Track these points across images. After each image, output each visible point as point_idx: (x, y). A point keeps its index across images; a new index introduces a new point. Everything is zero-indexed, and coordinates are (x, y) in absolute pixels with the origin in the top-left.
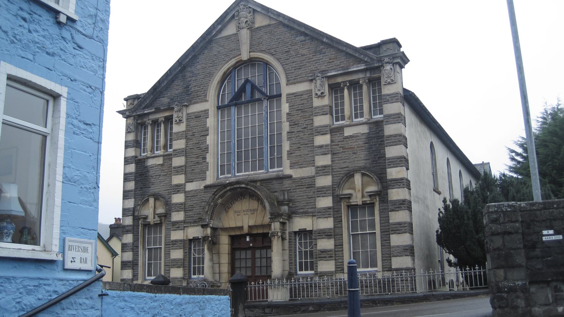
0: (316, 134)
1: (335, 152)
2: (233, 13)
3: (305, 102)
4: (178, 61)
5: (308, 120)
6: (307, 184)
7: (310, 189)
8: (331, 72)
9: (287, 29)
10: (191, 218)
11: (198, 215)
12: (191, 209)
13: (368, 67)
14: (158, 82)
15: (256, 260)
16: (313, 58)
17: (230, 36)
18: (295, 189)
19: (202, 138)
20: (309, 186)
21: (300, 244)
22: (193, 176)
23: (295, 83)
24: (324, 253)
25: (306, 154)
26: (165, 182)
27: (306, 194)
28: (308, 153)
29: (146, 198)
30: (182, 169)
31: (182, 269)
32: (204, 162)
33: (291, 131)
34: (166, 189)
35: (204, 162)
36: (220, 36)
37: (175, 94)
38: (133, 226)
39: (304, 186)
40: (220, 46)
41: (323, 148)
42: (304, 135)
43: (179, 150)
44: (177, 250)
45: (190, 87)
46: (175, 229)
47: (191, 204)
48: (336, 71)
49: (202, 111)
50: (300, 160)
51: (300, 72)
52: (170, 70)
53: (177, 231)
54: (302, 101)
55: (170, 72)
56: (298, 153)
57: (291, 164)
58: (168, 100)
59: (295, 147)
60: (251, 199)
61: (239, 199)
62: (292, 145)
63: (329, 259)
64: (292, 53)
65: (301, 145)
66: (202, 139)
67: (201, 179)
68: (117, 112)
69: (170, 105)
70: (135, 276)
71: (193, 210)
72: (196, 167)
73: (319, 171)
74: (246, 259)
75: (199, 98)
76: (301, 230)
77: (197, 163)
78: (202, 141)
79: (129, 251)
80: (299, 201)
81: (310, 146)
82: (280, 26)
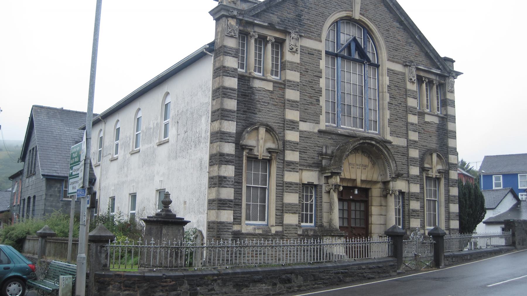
5: (402, 98)
6: (402, 152)
7: (404, 157)
10: (305, 161)
11: (312, 159)
12: (305, 151)
13: (442, 73)
15: (352, 211)
16: (405, 47)
23: (393, 62)
24: (414, 212)
26: (275, 113)
27: (401, 160)
29: (257, 126)
30: (297, 105)
34: (277, 122)
38: (236, 156)
39: (399, 153)
42: (399, 110)
43: (294, 82)
46: (290, 169)
47: (305, 146)
48: (423, 67)
49: (315, 50)
53: (292, 173)
54: (398, 80)
56: (395, 123)
58: (278, 20)
59: (394, 117)
62: (392, 115)
63: (418, 217)
64: (390, 33)
65: (398, 117)
66: (316, 80)
67: (316, 122)
68: (463, 73)
69: (286, 28)
70: (237, 220)
71: (306, 152)
78: (316, 82)
79: (230, 187)
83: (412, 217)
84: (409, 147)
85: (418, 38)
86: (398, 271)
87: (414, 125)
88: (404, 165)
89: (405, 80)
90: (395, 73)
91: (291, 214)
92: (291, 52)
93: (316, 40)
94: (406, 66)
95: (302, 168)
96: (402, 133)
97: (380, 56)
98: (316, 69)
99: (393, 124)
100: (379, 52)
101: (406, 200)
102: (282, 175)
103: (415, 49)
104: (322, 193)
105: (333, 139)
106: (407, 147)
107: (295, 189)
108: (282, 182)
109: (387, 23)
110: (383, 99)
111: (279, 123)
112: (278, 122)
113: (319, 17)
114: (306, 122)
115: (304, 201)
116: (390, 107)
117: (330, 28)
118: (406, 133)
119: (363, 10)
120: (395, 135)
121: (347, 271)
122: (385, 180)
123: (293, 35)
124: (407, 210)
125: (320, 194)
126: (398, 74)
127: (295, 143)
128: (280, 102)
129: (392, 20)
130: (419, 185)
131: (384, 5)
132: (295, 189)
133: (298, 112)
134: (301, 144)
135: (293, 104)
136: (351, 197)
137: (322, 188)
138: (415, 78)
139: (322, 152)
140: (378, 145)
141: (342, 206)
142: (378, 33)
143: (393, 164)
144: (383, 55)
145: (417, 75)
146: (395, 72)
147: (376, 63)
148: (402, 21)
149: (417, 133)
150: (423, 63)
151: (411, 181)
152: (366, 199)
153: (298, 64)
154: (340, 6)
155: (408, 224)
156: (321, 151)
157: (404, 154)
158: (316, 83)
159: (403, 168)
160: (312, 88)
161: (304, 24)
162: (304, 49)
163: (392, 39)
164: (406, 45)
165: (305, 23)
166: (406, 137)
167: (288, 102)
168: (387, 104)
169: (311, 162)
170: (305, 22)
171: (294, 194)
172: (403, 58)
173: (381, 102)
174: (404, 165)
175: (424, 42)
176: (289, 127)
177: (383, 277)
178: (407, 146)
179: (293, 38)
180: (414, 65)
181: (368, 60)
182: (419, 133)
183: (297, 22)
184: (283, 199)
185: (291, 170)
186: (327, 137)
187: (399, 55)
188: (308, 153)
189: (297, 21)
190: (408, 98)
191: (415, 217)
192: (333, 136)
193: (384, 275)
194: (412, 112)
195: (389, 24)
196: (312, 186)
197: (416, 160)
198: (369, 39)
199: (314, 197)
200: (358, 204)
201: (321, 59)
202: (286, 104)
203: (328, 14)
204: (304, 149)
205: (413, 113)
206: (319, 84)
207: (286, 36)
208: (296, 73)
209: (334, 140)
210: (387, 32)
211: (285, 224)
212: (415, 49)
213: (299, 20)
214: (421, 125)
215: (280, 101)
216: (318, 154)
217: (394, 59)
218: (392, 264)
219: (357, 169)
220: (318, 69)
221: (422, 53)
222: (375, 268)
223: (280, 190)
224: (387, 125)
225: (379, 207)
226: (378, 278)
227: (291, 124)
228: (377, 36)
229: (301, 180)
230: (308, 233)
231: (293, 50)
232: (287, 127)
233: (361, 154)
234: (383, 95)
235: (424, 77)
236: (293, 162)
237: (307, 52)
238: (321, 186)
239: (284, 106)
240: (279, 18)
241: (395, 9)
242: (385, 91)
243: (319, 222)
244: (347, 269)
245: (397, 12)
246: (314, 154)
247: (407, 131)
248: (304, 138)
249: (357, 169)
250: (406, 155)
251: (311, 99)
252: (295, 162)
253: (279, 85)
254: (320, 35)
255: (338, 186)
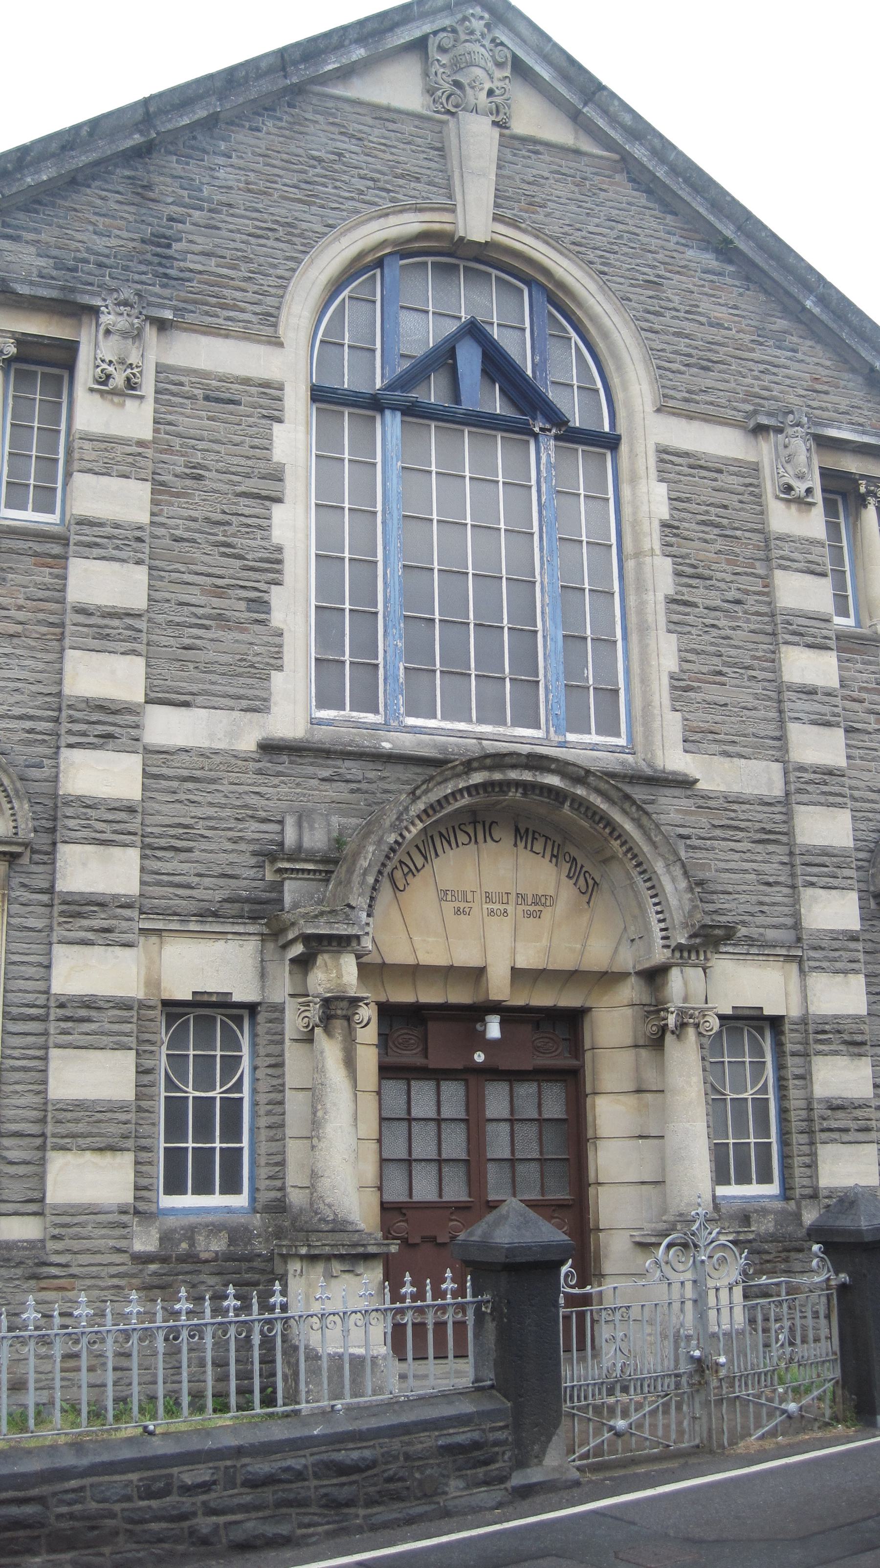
0: (789, 637)
1: (855, 725)
2: (427, 28)
3: (733, 500)
4: (146, 102)
5: (746, 574)
6: (758, 826)
7: (771, 848)
8: (839, 428)
9: (648, 200)
10: (180, 892)
11: (222, 882)
12: (179, 844)
14: (649, 125)
15: (490, 1128)
16: (753, 350)
17: (395, 116)
18: (709, 839)
19: (245, 506)
20: (767, 837)
21: (177, 1062)
22: (192, 680)
23: (690, 416)
24: (840, 1114)
25: (749, 705)
27: (754, 866)
28: (751, 702)
30: (130, 628)
31: (127, 1159)
32: (258, 621)
33: (679, 597)
34: (17, 711)
35: (258, 621)
36: (339, 91)
37: (88, 250)
40: (341, 133)
41: (815, 697)
43: (117, 526)
44: (98, 1053)
45: (176, 246)
49: (246, 381)
50: (723, 723)
51: (707, 380)
52: (95, 124)
55: (91, 134)
56: (713, 693)
57: (687, 729)
58: (42, 262)
60: (521, 845)
61: (462, 838)
63: (861, 1136)
64: (669, 294)
65: (725, 664)
66: (247, 511)
67: (244, 703)
69: (73, 290)
71: (190, 850)
72: (210, 634)
73: (806, 783)
74: (439, 1121)
75: (227, 313)
76: (740, 1012)
77: (220, 617)
80: (730, 888)
81: (764, 680)
82: (618, 177)
83: (825, 1136)
84: (794, 798)
85: (817, 310)
86: (517, 1479)
87: (818, 697)
88: (768, 884)
89: (759, 496)
90: (701, 467)
91: (88, 1155)
92: (101, 393)
93: (247, 337)
94: (759, 430)
95: (160, 925)
96: (755, 735)
97: (619, 396)
98: (250, 463)
99: (699, 696)
100: (615, 381)
101: (793, 1054)
102: (40, 965)
103: (808, 359)
104: (282, 1042)
105: (347, 781)
106: (786, 801)
107: (116, 1027)
108: (41, 1000)
109: (650, 255)
110: (641, 588)
111: (31, 718)
112: (24, 711)
113: (270, 243)
114: (186, 704)
115: (190, 1089)
116: (676, 618)
117: (345, 293)
118: (777, 734)
119: (516, 205)
120: (716, 748)
121: (29, 1510)
122: (647, 965)
123: (106, 319)
124: (802, 1104)
125: (272, 1049)
126: (720, 471)
127: (115, 809)
128: (39, 622)
129: (674, 239)
130: (861, 979)
131: (632, 180)
132: (116, 1027)
133: (139, 663)
134: (158, 813)
135: (106, 626)
136: (479, 1057)
137: (281, 1021)
138: (816, 482)
139: (281, 844)
140: (580, 791)
141: (433, 1103)
142: (600, 297)
143: (674, 880)
144: (635, 389)
145: (826, 473)
146: (702, 463)
147: (607, 428)
148: (727, 241)
149: (840, 732)
150: (855, 419)
151: (813, 964)
152: (570, 1062)
153: (141, 443)
154: (388, 191)
155: (808, 1171)
156: (272, 842)
157: (770, 832)
158: (249, 526)
159: (766, 899)
160: (223, 549)
161: (187, 275)
162: (183, 379)
163: (678, 318)
164: (761, 344)
165: (191, 271)
166: (778, 754)
167: (81, 619)
168: (661, 607)
169: (218, 896)
170: (192, 266)
171: (108, 1054)
172: (744, 401)
173: (632, 600)
174: (768, 884)
175: (848, 323)
176: (84, 734)
177: (374, 1528)
178: (787, 794)
179: (108, 332)
180: (798, 424)
181: (556, 418)
182: (849, 730)
183: (143, 268)
184: (45, 1082)
185: (90, 936)
186: (311, 770)
187: (720, 385)
188: (197, 853)
189: (150, 263)
190: (778, 574)
191: (846, 1137)
192: (348, 763)
193: (384, 1513)
194: (801, 635)
195: (659, 257)
196: (760, 1023)
197: (834, 859)
198: (565, 330)
199: (246, 1064)
200: (526, 1090)
201: (280, 421)
202: (70, 629)
203: (319, 228)
204: (172, 837)
205: (810, 640)
206: (267, 528)
207: (79, 325)
208: (132, 484)
209: (354, 786)
210: (651, 293)
211: (55, 1206)
212: (808, 359)
213: (156, 260)
214: (864, 695)
215: (41, 616)
216: (255, 854)
217: (692, 407)
218: (462, 1436)
219: (486, 919)
220: (262, 464)
221: (846, 376)
222: (300, 1476)
223: (31, 1039)
224: (666, 701)
225: (632, 1100)
226: (330, 1535)
227: (94, 719)
228: (598, 309)
229: (153, 982)
230: (192, 1245)
231: (112, 384)
232: (70, 732)
233: (507, 840)
234: (639, 566)
235: (863, 477)
236: (100, 899)
237: (198, 392)
238: (279, 1009)
239: (61, 638)
240: (48, 257)
241: (684, 193)
242: (647, 547)
243: (268, 1189)
244: (40, 1500)
245: (694, 205)
246: (232, 857)
247: (782, 724)
248: (175, 784)
249: (486, 919)
250: (784, 839)
251: (216, 602)
252: (115, 897)
253: (30, 544)
254: (271, 318)
255: (345, 1004)
